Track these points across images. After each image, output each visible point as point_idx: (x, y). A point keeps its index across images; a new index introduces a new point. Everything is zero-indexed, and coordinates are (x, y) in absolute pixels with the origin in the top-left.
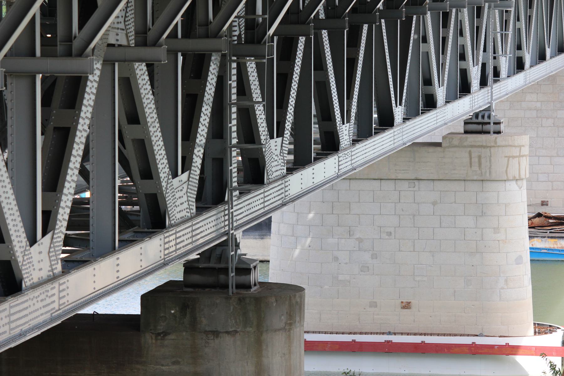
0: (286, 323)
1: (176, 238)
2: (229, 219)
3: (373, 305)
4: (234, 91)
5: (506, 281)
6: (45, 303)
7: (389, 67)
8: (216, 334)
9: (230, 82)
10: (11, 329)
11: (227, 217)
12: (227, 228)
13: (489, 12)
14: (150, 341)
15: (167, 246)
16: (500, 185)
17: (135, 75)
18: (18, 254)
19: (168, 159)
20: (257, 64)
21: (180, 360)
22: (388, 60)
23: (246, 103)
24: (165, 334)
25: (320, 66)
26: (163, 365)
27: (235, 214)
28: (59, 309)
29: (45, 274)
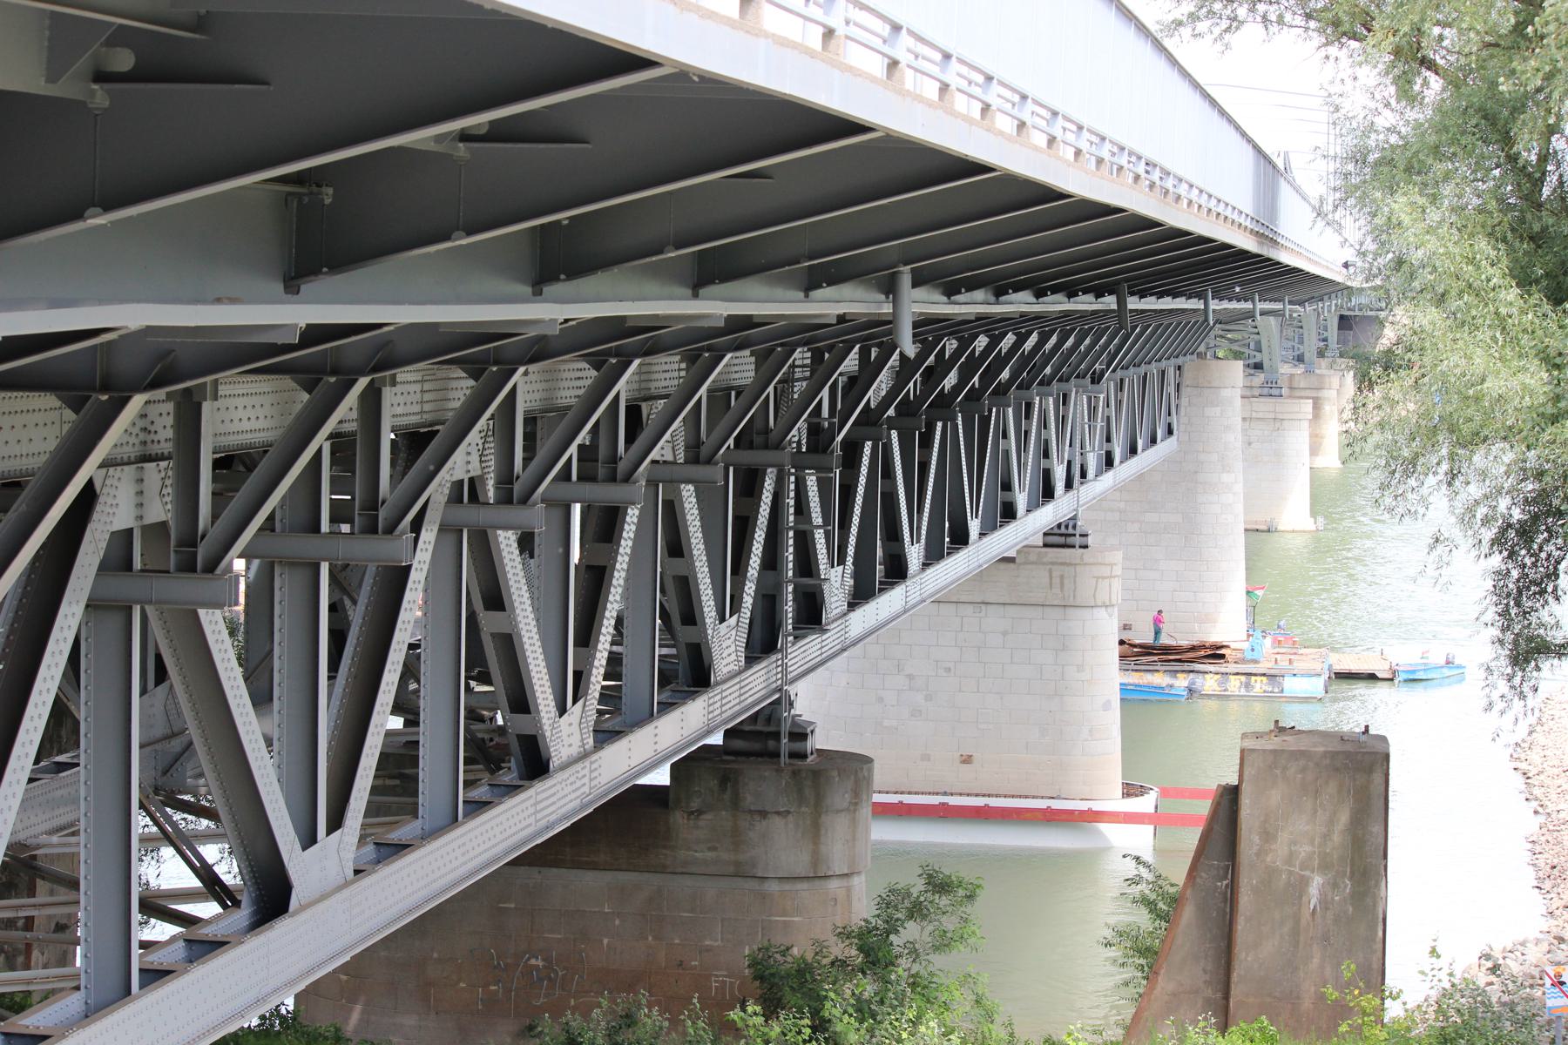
0: (850, 803)
1: (722, 698)
2: (782, 671)
3: (926, 757)
4: (792, 510)
5: (1090, 731)
6: (574, 787)
7: (965, 471)
8: (763, 814)
9: (787, 501)
10: (537, 821)
11: (780, 669)
12: (779, 682)
13: (1076, 398)
14: (681, 821)
15: (711, 709)
16: (1086, 613)
17: (681, 497)
18: (545, 728)
19: (715, 600)
20: (818, 479)
21: (717, 845)
22: (964, 463)
23: (802, 527)
24: (700, 812)
25: (888, 473)
26: (696, 851)
27: (789, 664)
28: (590, 794)
29: (575, 750)
